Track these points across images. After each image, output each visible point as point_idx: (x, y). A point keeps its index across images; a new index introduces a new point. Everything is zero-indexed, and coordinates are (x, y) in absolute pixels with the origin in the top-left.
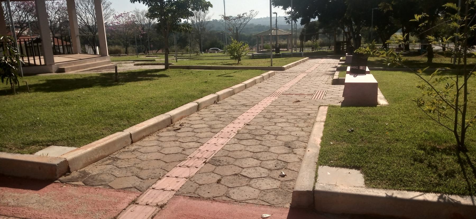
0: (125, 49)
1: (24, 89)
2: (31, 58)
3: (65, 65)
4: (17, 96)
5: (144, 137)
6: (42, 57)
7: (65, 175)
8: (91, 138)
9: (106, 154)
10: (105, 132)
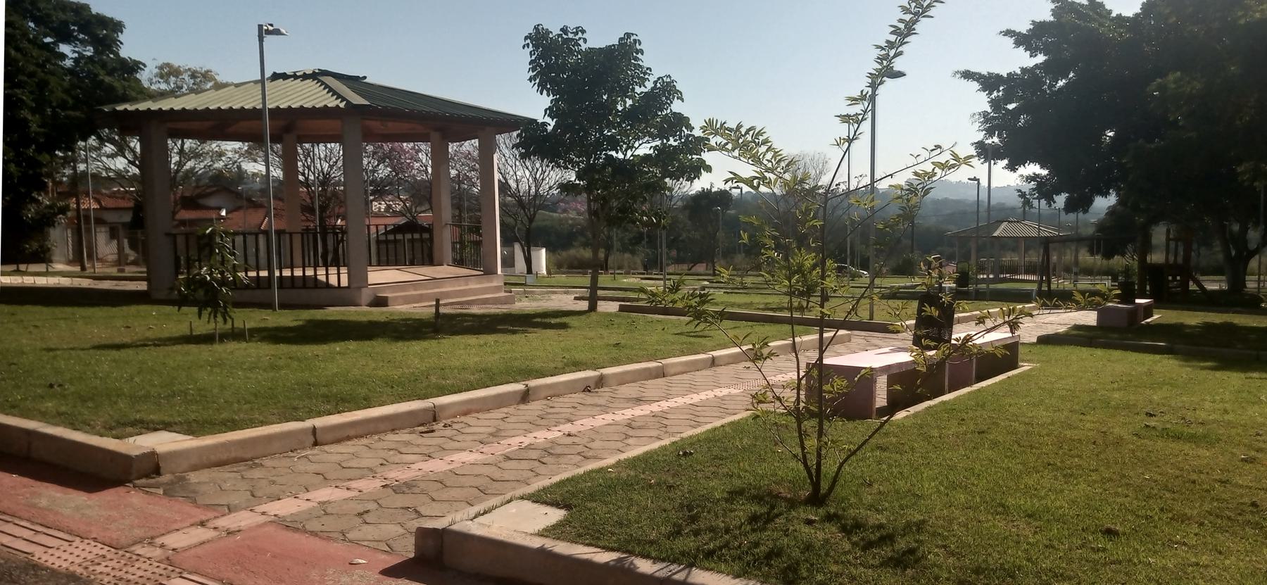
0: (1080, 258)
1: (237, 335)
2: (321, 272)
5: (349, 438)
6: (344, 270)
7: (147, 476)
8: (234, 425)
9: (249, 456)
10: (274, 418)
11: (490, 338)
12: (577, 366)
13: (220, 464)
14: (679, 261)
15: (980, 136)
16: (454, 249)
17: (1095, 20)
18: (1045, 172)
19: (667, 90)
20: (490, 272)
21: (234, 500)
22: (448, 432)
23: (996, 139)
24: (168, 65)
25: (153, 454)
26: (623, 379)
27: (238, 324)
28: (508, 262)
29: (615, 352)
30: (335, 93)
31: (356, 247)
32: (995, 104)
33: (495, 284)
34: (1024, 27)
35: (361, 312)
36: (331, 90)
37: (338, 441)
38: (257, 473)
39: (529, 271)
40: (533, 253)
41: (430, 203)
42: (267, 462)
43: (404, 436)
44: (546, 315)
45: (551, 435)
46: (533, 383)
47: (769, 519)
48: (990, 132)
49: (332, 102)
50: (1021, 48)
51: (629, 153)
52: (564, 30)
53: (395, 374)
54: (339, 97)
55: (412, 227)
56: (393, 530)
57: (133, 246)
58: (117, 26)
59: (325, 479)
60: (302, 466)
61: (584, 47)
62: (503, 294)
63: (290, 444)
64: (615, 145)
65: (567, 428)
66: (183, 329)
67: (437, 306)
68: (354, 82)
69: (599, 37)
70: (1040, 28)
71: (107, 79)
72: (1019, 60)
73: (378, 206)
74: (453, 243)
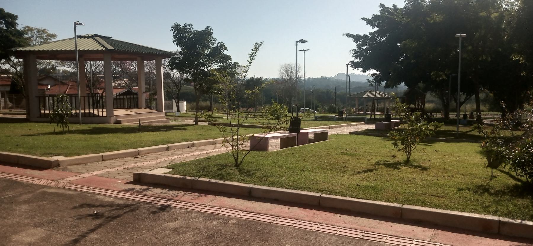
2: (96, 111)
3: (123, 117)
4: (64, 135)
5: (113, 159)
6: (104, 110)
7: (56, 167)
11: (158, 133)
12: (186, 140)
13: (76, 164)
14: (243, 107)
15: (353, 59)
16: (147, 102)
17: (395, 15)
18: (378, 73)
19: (222, 47)
20: (160, 111)
21: (83, 171)
22: (143, 158)
23: (358, 60)
24: (28, 27)
25: (57, 161)
26: (201, 145)
27: (71, 129)
28: (169, 107)
29: (199, 137)
30: (101, 44)
31: (110, 102)
32: (359, 47)
33: (162, 115)
34: (370, 17)
35: (112, 125)
36: (99, 43)
37: (109, 160)
38: (87, 167)
39: (178, 111)
40: (180, 104)
41: (137, 83)
42: (89, 164)
43: (129, 159)
44: (179, 126)
45: (173, 158)
46: (170, 145)
47: (222, 169)
48: (356, 57)
49: (100, 48)
50: (369, 25)
51: (209, 68)
52: (185, 25)
53: (126, 142)
54: (102, 46)
55: (129, 93)
56: (128, 176)
57: (11, 101)
58: (15, 17)
59: (107, 168)
60: (100, 165)
61: (192, 31)
62: (165, 119)
63: (95, 160)
64: (204, 65)
65: (180, 156)
66: (52, 130)
67: (140, 123)
68: (108, 39)
69: (198, 27)
70: (375, 17)
71: (13, 38)
72: (368, 30)
73: (115, 84)
74: (146, 100)
